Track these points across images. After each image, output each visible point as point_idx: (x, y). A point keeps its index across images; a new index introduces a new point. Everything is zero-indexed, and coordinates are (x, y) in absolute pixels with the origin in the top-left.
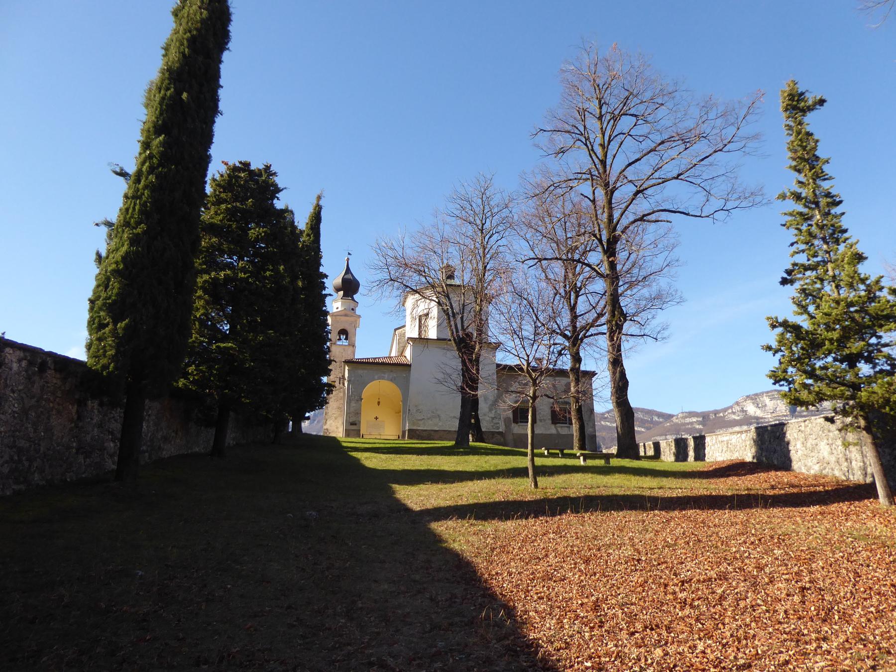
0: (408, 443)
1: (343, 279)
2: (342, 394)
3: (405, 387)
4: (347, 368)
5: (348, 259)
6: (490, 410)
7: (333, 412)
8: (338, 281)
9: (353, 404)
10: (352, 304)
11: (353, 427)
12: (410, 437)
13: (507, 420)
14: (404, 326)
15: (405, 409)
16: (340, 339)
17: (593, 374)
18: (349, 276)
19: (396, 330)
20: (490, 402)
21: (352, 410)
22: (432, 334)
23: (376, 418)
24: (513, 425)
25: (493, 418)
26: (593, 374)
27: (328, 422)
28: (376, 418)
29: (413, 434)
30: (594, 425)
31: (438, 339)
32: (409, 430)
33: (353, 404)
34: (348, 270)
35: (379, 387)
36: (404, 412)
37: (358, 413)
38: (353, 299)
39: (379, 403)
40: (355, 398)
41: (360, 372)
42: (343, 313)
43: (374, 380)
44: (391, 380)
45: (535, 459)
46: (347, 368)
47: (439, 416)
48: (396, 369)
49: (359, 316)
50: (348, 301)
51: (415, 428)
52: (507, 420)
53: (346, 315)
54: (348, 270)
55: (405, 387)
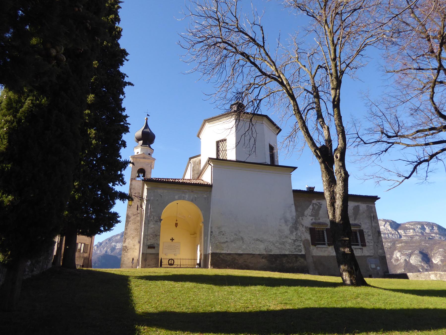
0: (211, 271)
1: (143, 132)
2: (139, 218)
3: (206, 209)
4: (146, 187)
5: (147, 119)
6: (292, 232)
7: (132, 232)
8: (139, 133)
9: (152, 225)
10: (149, 151)
11: (151, 255)
12: (215, 265)
13: (305, 242)
14: (199, 156)
15: (205, 229)
16: (139, 176)
17: (376, 198)
18: (147, 130)
19: (190, 159)
20: (290, 225)
21: (150, 231)
22: (231, 155)
23: (172, 239)
24: (312, 247)
25: (295, 241)
26: (376, 198)
27: (127, 241)
28: (172, 239)
29: (219, 260)
30: (382, 246)
31: (237, 161)
32: (212, 254)
33: (152, 225)
34: (147, 126)
35: (179, 208)
36: (206, 235)
37: (157, 235)
38: (150, 147)
39: (176, 225)
40: (154, 219)
41: (160, 191)
42: (142, 156)
43: (174, 200)
44: (192, 201)
45: (342, 281)
46: (146, 187)
47: (242, 238)
48: (197, 190)
49: (154, 159)
50: (146, 148)
51: (218, 251)
52: (305, 242)
53: (144, 158)
54: (147, 126)
55: (206, 209)
